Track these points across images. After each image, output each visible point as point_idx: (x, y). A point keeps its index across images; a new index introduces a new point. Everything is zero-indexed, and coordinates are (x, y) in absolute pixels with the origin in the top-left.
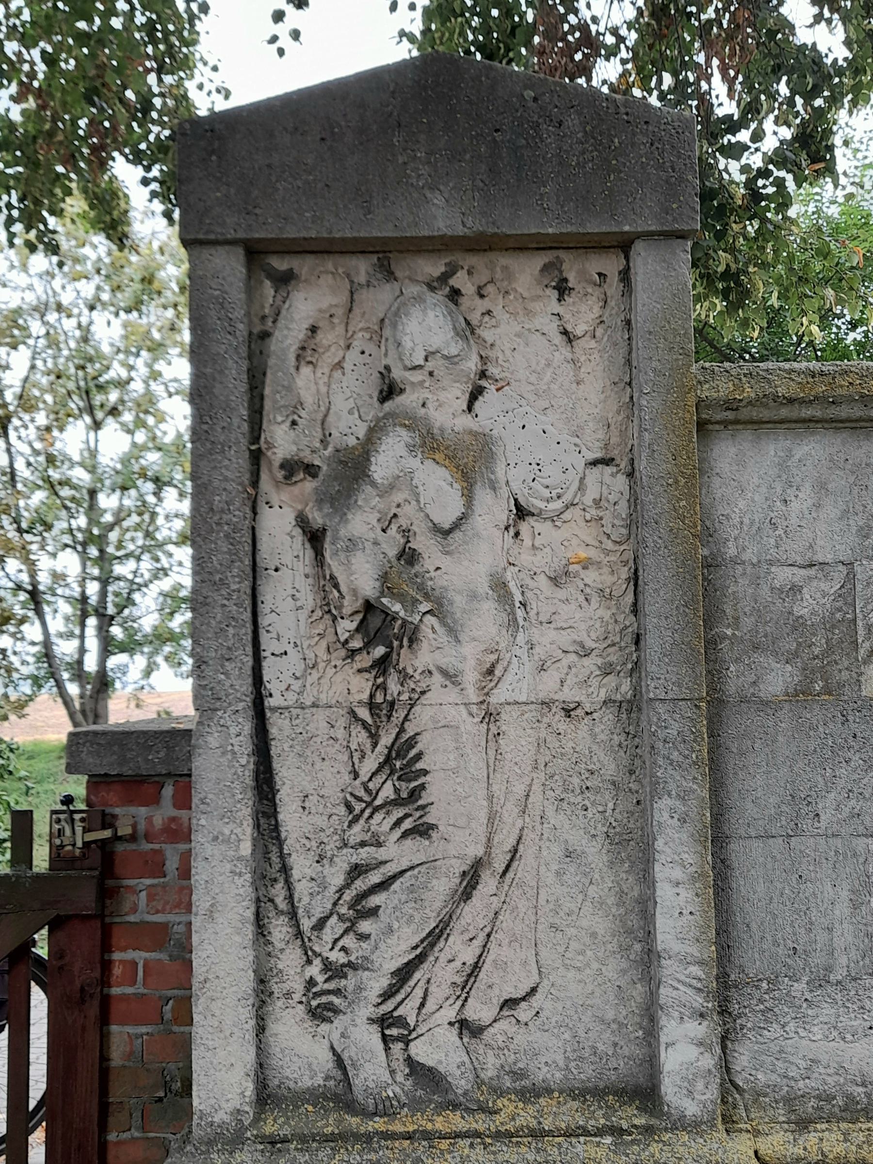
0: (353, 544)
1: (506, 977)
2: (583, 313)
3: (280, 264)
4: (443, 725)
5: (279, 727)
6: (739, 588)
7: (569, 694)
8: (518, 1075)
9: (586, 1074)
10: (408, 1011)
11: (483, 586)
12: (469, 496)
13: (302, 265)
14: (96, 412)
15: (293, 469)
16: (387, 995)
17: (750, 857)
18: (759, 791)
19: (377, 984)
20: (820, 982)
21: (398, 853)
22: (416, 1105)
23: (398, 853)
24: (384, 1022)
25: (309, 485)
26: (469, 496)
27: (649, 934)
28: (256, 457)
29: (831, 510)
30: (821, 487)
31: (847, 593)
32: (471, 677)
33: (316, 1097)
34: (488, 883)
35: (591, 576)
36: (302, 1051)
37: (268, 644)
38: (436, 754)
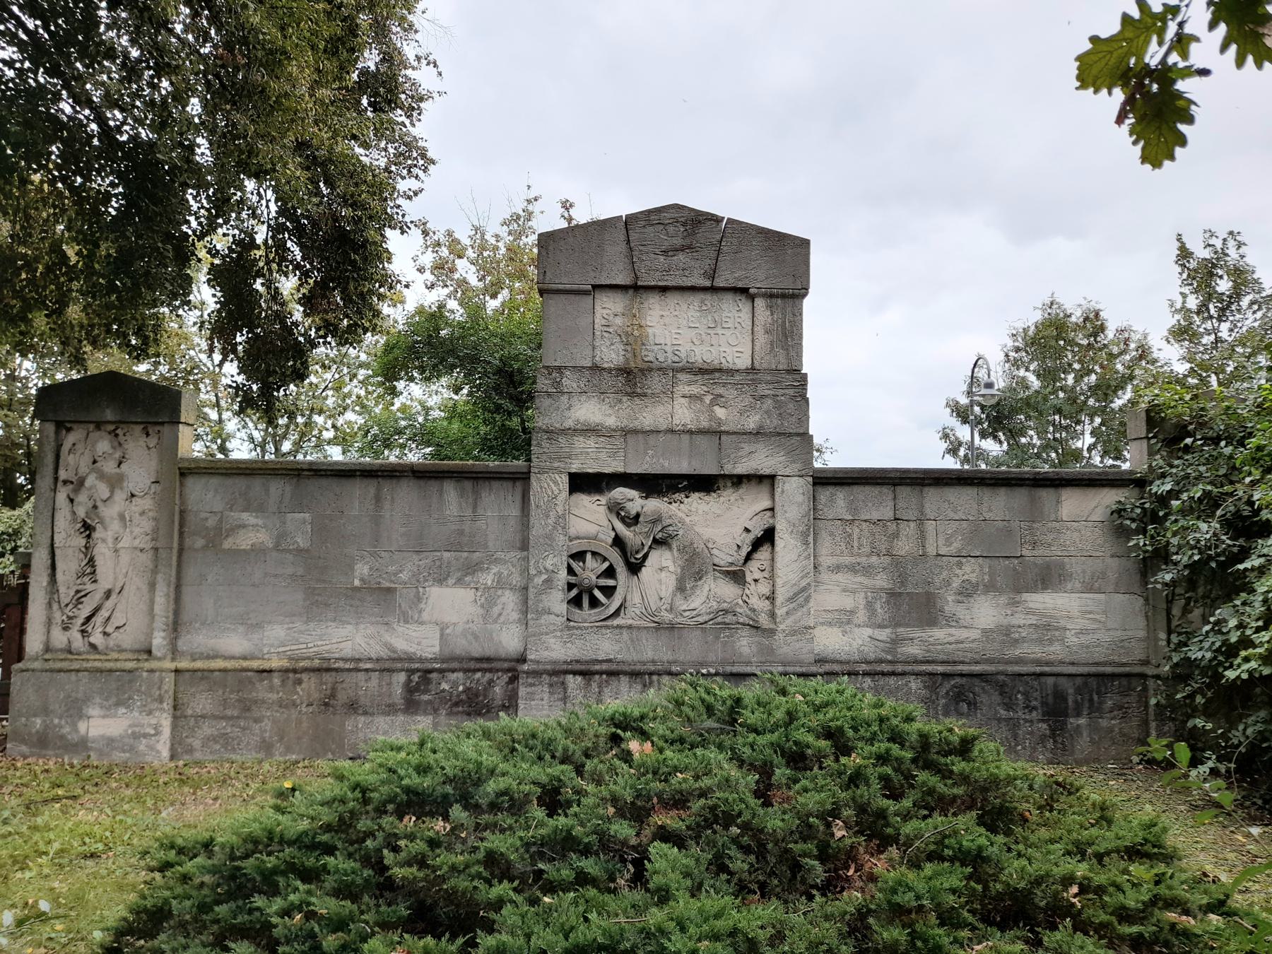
0: (79, 503)
1: (118, 620)
2: (152, 441)
3: (68, 425)
4: (102, 552)
5: (58, 552)
6: (190, 518)
7: (142, 546)
8: (118, 646)
9: (137, 646)
10: (89, 629)
11: (115, 516)
12: (112, 492)
13: (75, 426)
14: (53, 627)
15: (65, 482)
16: (83, 624)
17: (188, 592)
18: (191, 573)
19: (80, 621)
20: (203, 624)
21: (89, 587)
22: (88, 653)
23: (89, 587)
24: (83, 631)
25: (71, 486)
26: (112, 492)
27: (152, 609)
28: (56, 479)
29: (218, 498)
30: (216, 491)
31: (221, 521)
32: (110, 540)
33: (61, 650)
34: (114, 596)
35: (151, 514)
36: (59, 639)
37: (56, 529)
38: (99, 561)
